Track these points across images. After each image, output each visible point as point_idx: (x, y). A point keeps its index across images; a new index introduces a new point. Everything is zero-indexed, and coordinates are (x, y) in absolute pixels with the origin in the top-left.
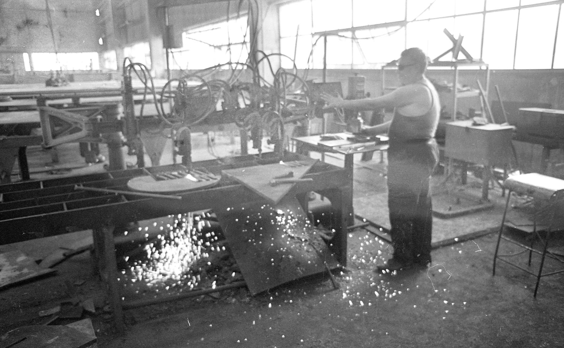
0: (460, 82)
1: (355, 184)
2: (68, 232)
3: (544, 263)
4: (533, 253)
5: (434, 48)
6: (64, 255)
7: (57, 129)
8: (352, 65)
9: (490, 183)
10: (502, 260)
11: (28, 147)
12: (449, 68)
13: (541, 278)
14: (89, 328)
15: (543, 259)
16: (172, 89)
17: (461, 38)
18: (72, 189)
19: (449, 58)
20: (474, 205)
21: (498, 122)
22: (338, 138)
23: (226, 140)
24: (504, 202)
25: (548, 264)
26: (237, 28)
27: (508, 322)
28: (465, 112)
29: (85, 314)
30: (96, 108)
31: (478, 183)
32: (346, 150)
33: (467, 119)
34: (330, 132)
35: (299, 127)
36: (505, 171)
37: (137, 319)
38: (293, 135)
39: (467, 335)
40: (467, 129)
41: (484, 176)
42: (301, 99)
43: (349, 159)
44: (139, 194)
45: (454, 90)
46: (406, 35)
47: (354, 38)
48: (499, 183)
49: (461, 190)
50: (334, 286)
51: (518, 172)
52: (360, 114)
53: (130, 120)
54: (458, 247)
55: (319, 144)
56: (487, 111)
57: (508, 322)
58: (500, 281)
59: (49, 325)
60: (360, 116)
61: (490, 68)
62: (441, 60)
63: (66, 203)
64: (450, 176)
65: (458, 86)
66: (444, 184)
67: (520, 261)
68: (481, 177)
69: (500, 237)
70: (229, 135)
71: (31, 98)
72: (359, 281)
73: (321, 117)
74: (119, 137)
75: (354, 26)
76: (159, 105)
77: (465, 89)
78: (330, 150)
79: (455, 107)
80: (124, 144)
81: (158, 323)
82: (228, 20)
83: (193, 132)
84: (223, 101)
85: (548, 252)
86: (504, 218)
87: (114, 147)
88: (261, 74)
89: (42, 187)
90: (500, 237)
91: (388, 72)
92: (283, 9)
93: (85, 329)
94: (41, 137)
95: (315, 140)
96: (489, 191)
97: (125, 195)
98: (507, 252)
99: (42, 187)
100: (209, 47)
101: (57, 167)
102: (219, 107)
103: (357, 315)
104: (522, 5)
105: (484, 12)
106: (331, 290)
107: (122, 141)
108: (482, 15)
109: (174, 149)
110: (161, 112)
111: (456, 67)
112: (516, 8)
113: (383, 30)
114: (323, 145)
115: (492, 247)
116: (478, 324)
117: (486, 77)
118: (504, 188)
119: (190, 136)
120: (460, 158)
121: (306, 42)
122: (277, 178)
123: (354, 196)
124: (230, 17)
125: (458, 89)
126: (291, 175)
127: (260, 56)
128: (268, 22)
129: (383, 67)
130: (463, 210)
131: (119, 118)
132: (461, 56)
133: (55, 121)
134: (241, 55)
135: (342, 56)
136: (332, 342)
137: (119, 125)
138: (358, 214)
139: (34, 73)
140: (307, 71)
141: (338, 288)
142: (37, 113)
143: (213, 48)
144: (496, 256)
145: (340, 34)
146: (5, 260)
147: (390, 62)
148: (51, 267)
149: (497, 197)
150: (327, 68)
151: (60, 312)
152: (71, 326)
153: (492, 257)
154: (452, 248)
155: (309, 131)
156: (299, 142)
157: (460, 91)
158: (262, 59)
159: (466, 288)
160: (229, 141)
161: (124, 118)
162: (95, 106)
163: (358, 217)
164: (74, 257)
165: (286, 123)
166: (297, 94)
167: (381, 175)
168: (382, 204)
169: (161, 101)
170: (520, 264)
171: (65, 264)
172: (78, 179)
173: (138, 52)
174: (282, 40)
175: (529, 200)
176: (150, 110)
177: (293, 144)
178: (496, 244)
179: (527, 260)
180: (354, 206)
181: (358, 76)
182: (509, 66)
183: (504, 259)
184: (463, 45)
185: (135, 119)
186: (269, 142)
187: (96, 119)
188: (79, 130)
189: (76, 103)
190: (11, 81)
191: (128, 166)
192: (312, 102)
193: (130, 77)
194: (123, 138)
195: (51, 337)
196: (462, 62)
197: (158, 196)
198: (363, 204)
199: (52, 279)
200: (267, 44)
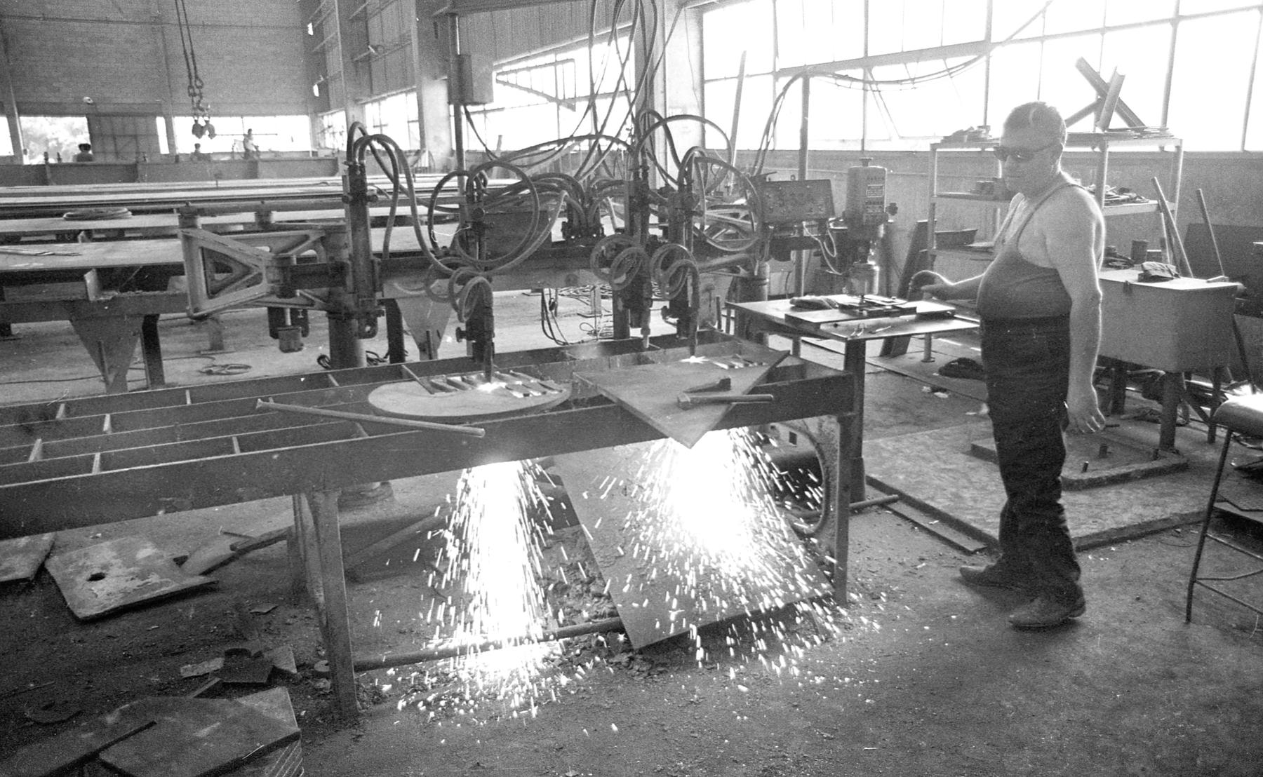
0: (1111, 183)
1: (868, 409)
2: (240, 500)
5: (1070, 99)
6: (232, 548)
7: (219, 277)
9: (1180, 411)
11: (163, 316)
14: (284, 707)
20: (1141, 461)
21: (1199, 274)
24: (1212, 455)
26: (605, 61)
27: (1223, 732)
28: (1127, 253)
29: (276, 677)
33: (1128, 265)
34: (811, 293)
35: (743, 280)
36: (1217, 385)
38: (729, 298)
39: (1124, 758)
40: (1127, 287)
41: (1168, 396)
43: (855, 351)
44: (393, 420)
48: (1202, 413)
51: (1246, 389)
52: (872, 253)
54: (1104, 555)
55: (787, 316)
57: (1223, 732)
58: (1202, 635)
59: (199, 696)
60: (873, 258)
61: (1185, 148)
63: (239, 439)
67: (1252, 592)
68: (1158, 399)
69: (1203, 537)
71: (170, 211)
76: (424, 229)
77: (1123, 197)
78: (815, 330)
84: (566, 220)
86: (1215, 491)
89: (189, 402)
90: (1203, 537)
91: (947, 158)
92: (708, 17)
94: (185, 295)
95: (779, 309)
96: (1178, 429)
98: (1217, 570)
99: (189, 402)
100: (540, 104)
102: (557, 234)
104: (1046, 33)
105: (1176, 20)
108: (1168, 27)
110: (429, 245)
111: (1103, 149)
112: (1109, 29)
113: (937, 65)
115: (1183, 559)
118: (1212, 423)
122: (693, 391)
125: (1108, 196)
126: (725, 384)
128: (678, 51)
129: (934, 146)
132: (1117, 122)
133: (219, 263)
134: (618, 120)
135: (839, 124)
139: (177, 157)
142: (177, 243)
144: (1193, 580)
146: (114, 554)
148: (206, 573)
149: (1200, 444)
150: (810, 147)
153: (1185, 581)
159: (1123, 650)
162: (301, 228)
163: (874, 483)
164: (251, 555)
165: (702, 270)
166: (738, 207)
167: (926, 389)
168: (928, 455)
171: (232, 567)
173: (393, 116)
176: (403, 239)
177: (728, 317)
178: (1194, 551)
182: (1228, 143)
184: (1123, 96)
185: (373, 257)
188: (256, 281)
189: (264, 224)
190: (131, 173)
191: (369, 360)
192: (764, 225)
195: (204, 723)
196: (1119, 135)
198: (885, 454)
199: (210, 598)
200: (675, 93)
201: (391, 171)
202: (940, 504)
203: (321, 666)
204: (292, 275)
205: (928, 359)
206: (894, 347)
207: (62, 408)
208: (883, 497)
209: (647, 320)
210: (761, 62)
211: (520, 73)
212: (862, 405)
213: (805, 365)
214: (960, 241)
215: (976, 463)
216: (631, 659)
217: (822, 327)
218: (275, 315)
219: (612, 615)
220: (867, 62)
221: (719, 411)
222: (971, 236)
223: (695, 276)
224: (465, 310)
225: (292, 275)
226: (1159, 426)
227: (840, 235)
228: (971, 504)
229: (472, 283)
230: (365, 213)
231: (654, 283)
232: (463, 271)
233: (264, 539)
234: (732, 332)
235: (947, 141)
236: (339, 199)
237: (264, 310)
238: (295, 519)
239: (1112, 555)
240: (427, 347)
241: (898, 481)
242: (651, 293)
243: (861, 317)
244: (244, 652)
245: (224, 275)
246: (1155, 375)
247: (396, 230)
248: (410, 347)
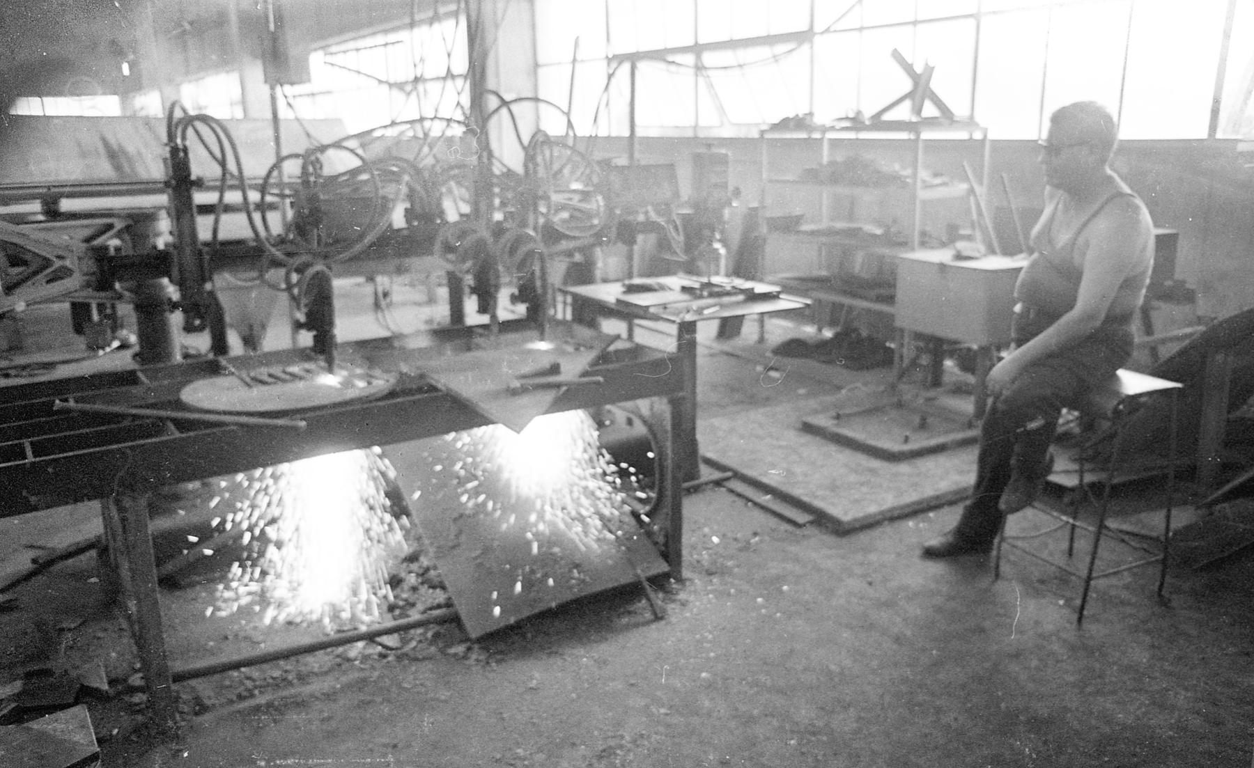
2: (35, 509)
3: (1099, 551)
4: (1077, 531)
6: (34, 561)
8: (695, 127)
10: (1014, 546)
12: (903, 135)
13: (1092, 583)
15: (1097, 540)
16: (286, 180)
17: (929, 70)
18: (47, 409)
19: (903, 113)
21: (1009, 251)
22: (662, 288)
23: (419, 295)
25: (1108, 551)
26: (440, 44)
29: (85, 694)
30: (109, 221)
31: (967, 385)
32: (678, 314)
33: (943, 245)
34: (649, 275)
35: (576, 264)
37: (208, 702)
38: (565, 283)
39: (938, 711)
40: (942, 267)
42: (580, 201)
43: (687, 329)
45: (915, 183)
46: (812, 61)
47: (699, 68)
49: (929, 399)
50: (655, 614)
53: (188, 250)
55: (619, 301)
56: (984, 230)
60: (720, 241)
61: (991, 136)
62: (887, 117)
63: (32, 443)
64: (908, 369)
65: (923, 174)
66: (893, 387)
67: (1051, 547)
70: (423, 283)
72: (710, 602)
73: (631, 242)
74: (162, 288)
75: (701, 41)
76: (257, 217)
77: (938, 181)
78: (644, 313)
79: (917, 223)
80: (174, 306)
81: (257, 709)
82: (412, 25)
83: (339, 275)
84: (408, 206)
85: (1106, 527)
87: (151, 312)
88: (494, 145)
93: (74, 728)
95: (609, 293)
97: (175, 421)
98: (1024, 530)
101: (21, 360)
103: (704, 675)
106: (648, 623)
107: (170, 299)
109: (292, 316)
113: (764, 52)
114: (627, 304)
116: (963, 687)
117: (982, 156)
119: (330, 286)
120: (928, 330)
121: (593, 74)
122: (524, 377)
123: (699, 413)
124: (417, 17)
125: (924, 181)
126: (555, 369)
127: (493, 102)
130: (933, 442)
131: (161, 245)
132: (929, 110)
134: (451, 101)
136: (649, 737)
137: (160, 263)
138: (710, 455)
140: (592, 140)
141: (662, 618)
143: (386, 87)
145: (670, 58)
147: (777, 121)
150: (640, 132)
151: (19, 695)
152: (36, 725)
154: (911, 524)
155: (598, 274)
156: (576, 297)
157: (928, 186)
158: (497, 110)
160: (423, 298)
161: (175, 246)
163: (708, 462)
164: (59, 566)
166: (574, 191)
167: (759, 368)
168: (761, 432)
169: (262, 207)
170: (1051, 554)
172: (62, 387)
174: (541, 71)
175: (1071, 418)
176: (234, 227)
177: (565, 303)
179: (1065, 545)
180: (699, 437)
181: (715, 150)
183: (1019, 543)
184: (934, 85)
186: (514, 299)
187: (106, 248)
189: (53, 213)
193: (185, 150)
194: (172, 291)
196: (931, 122)
197: (261, 421)
198: (720, 433)
200: (507, 76)
201: (218, 155)
202: (773, 477)
203: (136, 680)
204: (107, 270)
205: (762, 340)
206: (729, 327)
207: (475, 483)
208: (717, 475)
209: (495, 307)
210: (595, 50)
211: (349, 54)
212: (694, 386)
213: (638, 350)
214: (788, 225)
215: (807, 438)
216: (469, 649)
217: (652, 310)
218: (80, 312)
219: (449, 604)
220: (697, 49)
221: (549, 396)
222: (798, 219)
223: (542, 260)
224: (304, 301)
225: (107, 270)
226: (972, 398)
227: (687, 220)
228: (800, 478)
229: (311, 272)
230: (190, 198)
231: (500, 268)
232: (298, 261)
233: (71, 549)
234: (569, 317)
235: (775, 127)
236: (161, 185)
237: (67, 306)
238: (106, 527)
239: (930, 521)
240: (250, 341)
241: (731, 460)
242: (498, 277)
243: (701, 297)
244: (47, 673)
245: (21, 269)
246: (969, 350)
247: (225, 218)
248: (234, 341)
